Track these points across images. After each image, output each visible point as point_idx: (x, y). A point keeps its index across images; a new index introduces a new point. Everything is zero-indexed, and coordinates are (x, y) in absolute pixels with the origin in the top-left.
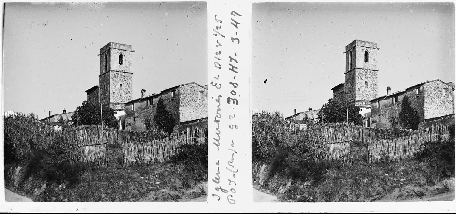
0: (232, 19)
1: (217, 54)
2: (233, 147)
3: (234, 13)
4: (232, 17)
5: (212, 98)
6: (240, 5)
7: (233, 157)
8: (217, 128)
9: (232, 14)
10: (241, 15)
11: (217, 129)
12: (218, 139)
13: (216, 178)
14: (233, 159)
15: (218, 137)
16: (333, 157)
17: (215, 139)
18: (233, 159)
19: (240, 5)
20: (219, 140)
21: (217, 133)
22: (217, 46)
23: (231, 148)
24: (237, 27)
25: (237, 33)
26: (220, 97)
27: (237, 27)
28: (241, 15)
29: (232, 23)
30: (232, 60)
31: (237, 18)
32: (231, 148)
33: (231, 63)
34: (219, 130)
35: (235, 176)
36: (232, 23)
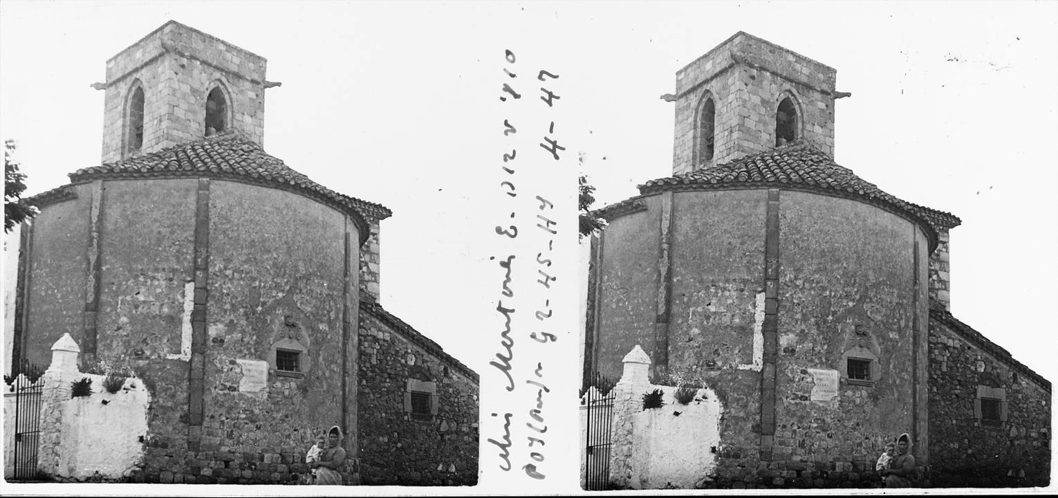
0: (542, 89)
1: (506, 157)
2: (540, 376)
3: (544, 76)
4: (541, 84)
5: (492, 258)
6: (556, 13)
7: (542, 399)
8: (505, 434)
9: (540, 77)
10: (556, 77)
11: (504, 334)
12: (507, 356)
13: (499, 356)
14: (540, 406)
15: (505, 461)
16: (602, 444)
17: (499, 356)
18: (540, 406)
19: (556, 13)
20: (510, 358)
21: (501, 455)
22: (506, 133)
23: (535, 378)
24: (551, 105)
25: (548, 301)
26: (511, 387)
27: (551, 105)
28: (556, 77)
29: (542, 145)
30: (535, 442)
31: (549, 84)
32: (535, 378)
33: (542, 213)
34: (510, 374)
35: (552, 245)
36: (542, 145)
